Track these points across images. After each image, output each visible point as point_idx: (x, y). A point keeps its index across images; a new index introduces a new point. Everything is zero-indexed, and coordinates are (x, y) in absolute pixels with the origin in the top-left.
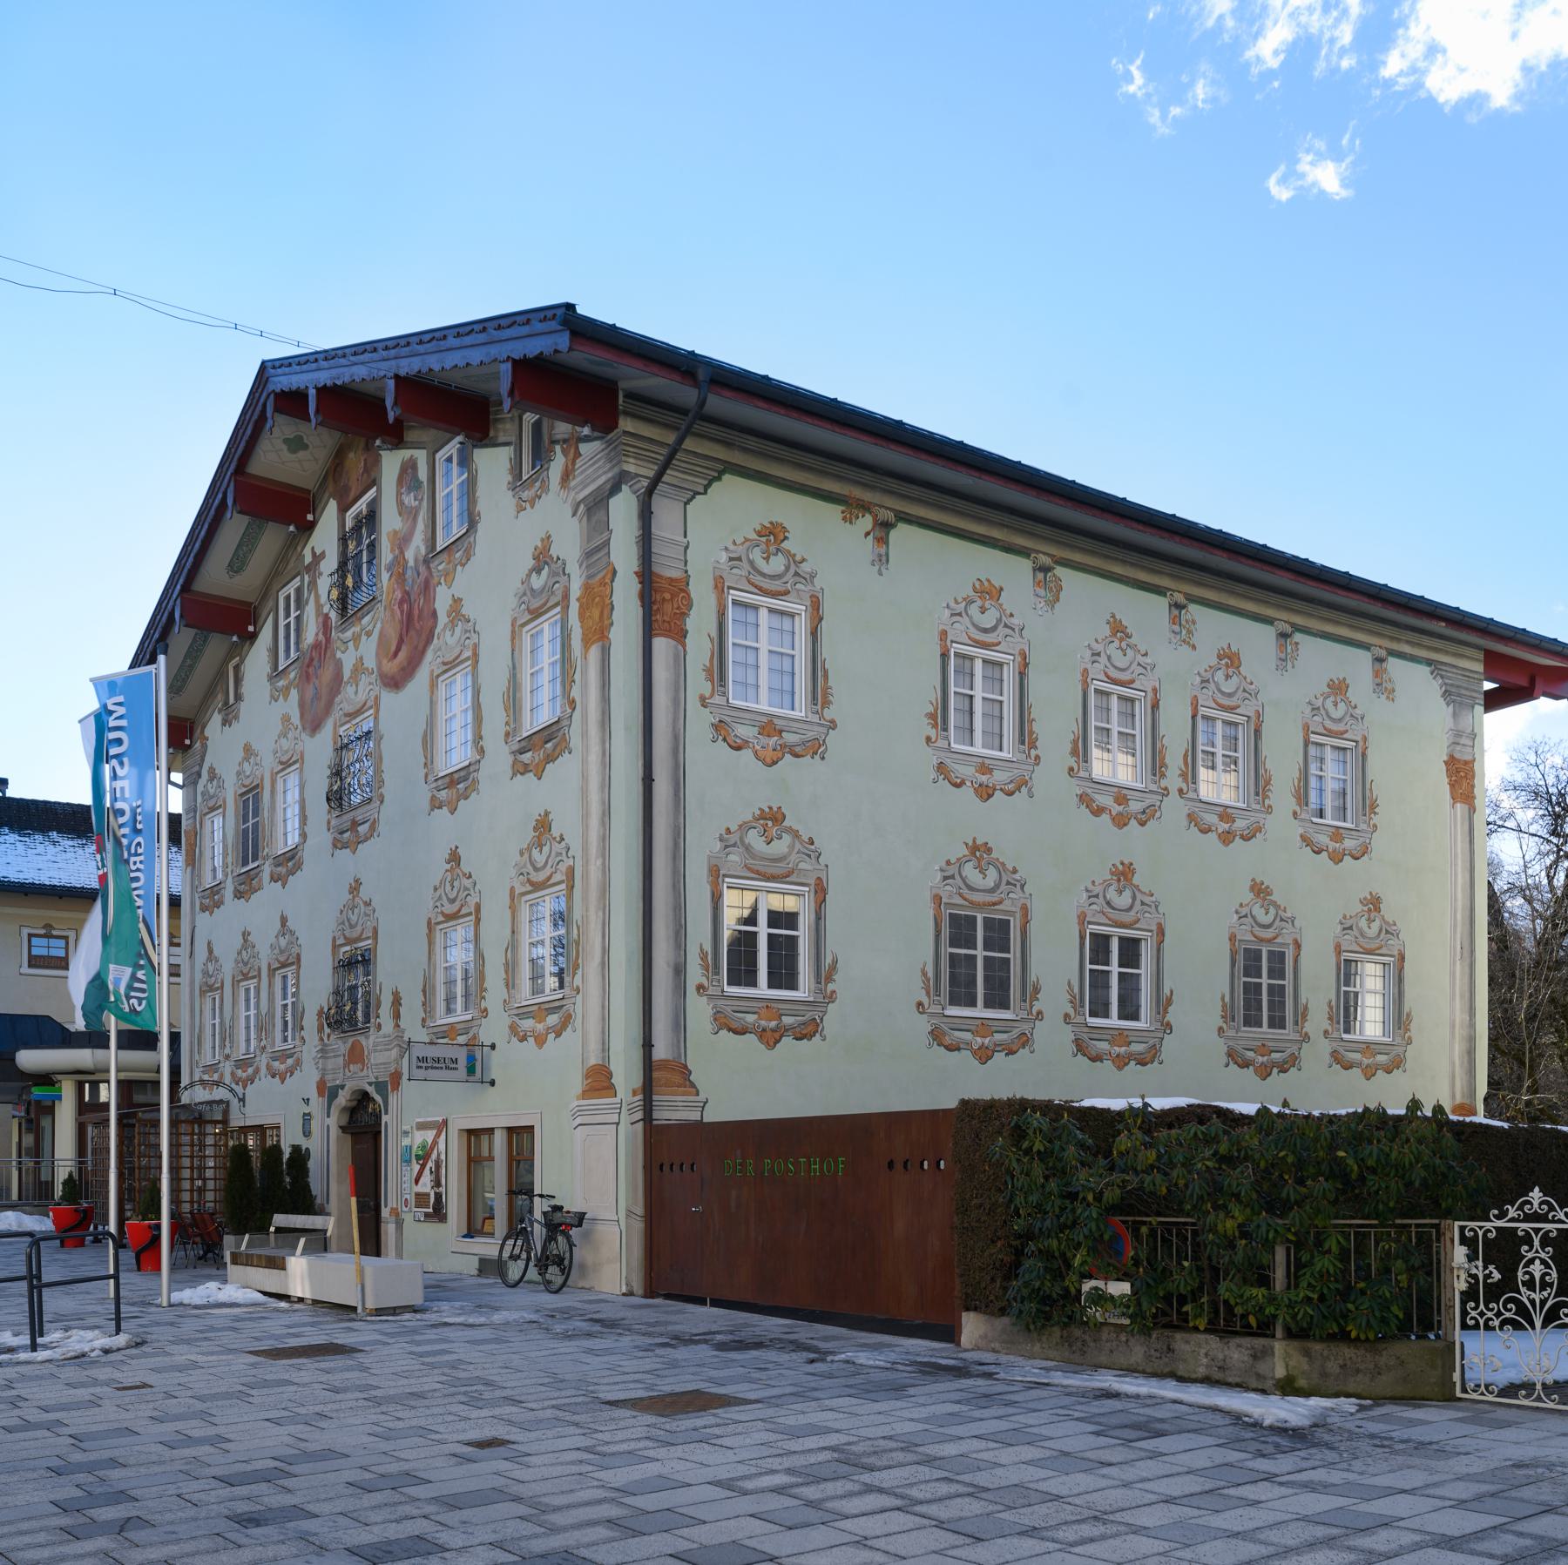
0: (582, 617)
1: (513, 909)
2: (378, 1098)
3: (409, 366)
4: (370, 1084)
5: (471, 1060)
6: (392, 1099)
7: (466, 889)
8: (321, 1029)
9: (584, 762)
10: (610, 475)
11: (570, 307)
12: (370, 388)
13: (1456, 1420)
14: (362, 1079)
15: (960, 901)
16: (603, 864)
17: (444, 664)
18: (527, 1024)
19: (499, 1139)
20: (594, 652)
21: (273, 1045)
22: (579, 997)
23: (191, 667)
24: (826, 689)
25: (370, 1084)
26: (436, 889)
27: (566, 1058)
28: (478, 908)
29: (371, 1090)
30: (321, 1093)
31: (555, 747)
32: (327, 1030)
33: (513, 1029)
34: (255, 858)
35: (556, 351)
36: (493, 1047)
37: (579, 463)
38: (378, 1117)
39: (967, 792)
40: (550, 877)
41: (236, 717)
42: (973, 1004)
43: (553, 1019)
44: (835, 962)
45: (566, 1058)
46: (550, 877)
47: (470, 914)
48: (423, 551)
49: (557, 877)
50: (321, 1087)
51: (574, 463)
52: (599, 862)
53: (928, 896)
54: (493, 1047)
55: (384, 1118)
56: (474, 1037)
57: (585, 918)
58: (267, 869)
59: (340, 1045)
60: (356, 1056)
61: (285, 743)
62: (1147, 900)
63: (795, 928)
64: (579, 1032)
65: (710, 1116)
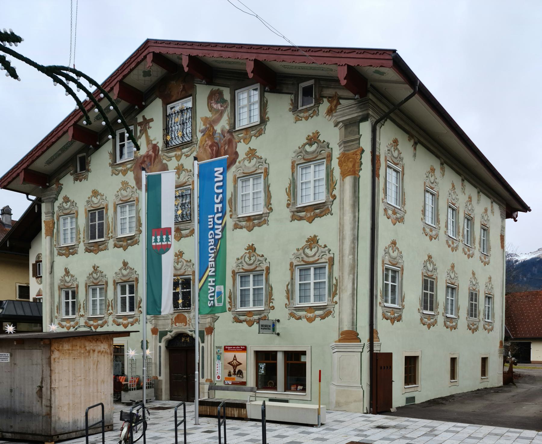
0: (340, 164)
3: (194, 53)
7: (259, 260)
9: (341, 219)
10: (360, 114)
11: (394, 51)
12: (175, 58)
13: (251, 426)
15: (302, 263)
16: (354, 258)
17: (244, 173)
19: (280, 358)
20: (349, 180)
21: (117, 313)
22: (337, 306)
23: (60, 154)
26: (238, 259)
27: (329, 329)
28: (268, 269)
31: (321, 212)
34: (101, 236)
35: (358, 65)
37: (339, 107)
39: (428, 237)
40: (318, 260)
41: (86, 178)
42: (190, 291)
45: (329, 329)
46: (318, 260)
48: (227, 127)
51: (336, 106)
52: (351, 257)
53: (421, 273)
54: (278, 321)
56: (265, 316)
57: (342, 277)
58: (111, 243)
61: (124, 193)
62: (261, 259)
64: (337, 318)
65: (382, 351)
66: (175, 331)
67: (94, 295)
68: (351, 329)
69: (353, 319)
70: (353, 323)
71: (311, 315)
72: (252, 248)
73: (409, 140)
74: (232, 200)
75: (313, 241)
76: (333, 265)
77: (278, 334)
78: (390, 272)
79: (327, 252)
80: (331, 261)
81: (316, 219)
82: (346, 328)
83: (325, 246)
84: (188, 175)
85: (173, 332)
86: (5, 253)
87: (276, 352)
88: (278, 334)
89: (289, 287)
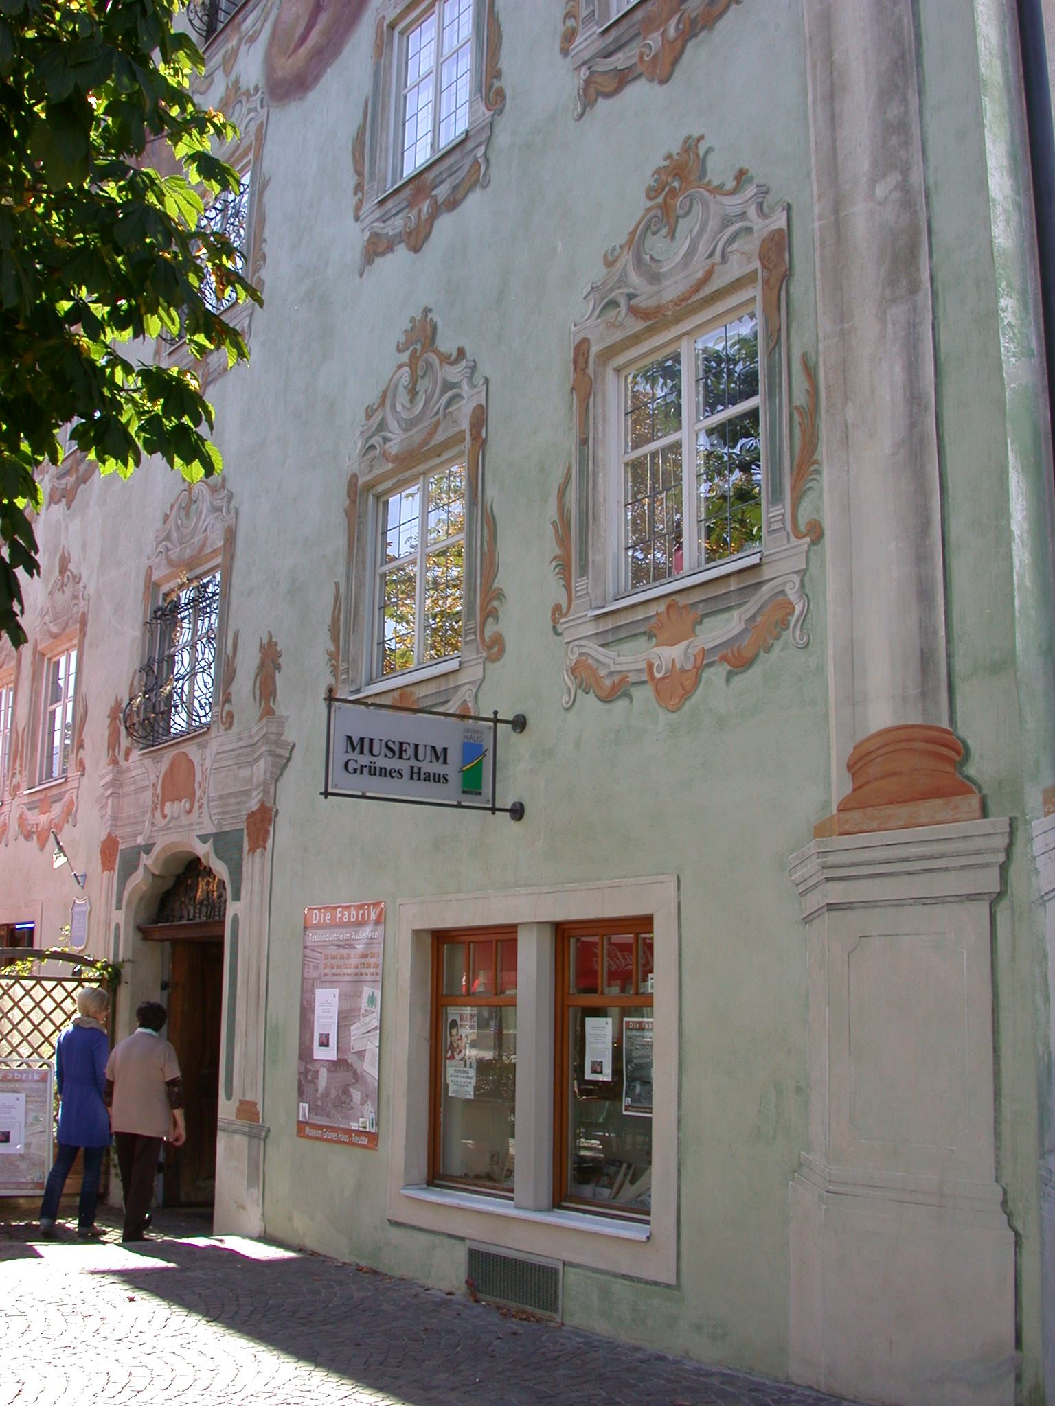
1: (584, 390)
2: (220, 868)
4: (204, 839)
5: (473, 751)
6: (252, 866)
7: (447, 386)
8: (113, 743)
14: (189, 831)
18: (628, 658)
24: (563, 541)
25: (204, 839)
28: (480, 417)
29: (203, 850)
30: (107, 863)
32: (125, 741)
33: (584, 676)
36: (520, 724)
38: (216, 909)
43: (723, 628)
44: (37, 1255)
47: (458, 438)
49: (735, 269)
50: (109, 849)
54: (520, 724)
55: (232, 908)
59: (144, 769)
60: (179, 785)
63: (498, 942)
66: (161, 842)
67: (652, 419)
68: (914, 719)
69: (926, 630)
70: (926, 660)
71: (670, 655)
72: (422, 336)
73: (650, 1045)
74: (363, 134)
75: (680, 178)
76: (787, 276)
77: (517, 812)
78: (428, 550)
79: (752, 211)
80: (777, 251)
81: (690, 44)
82: (881, 715)
83: (742, 176)
84: (250, 111)
85: (156, 850)
86: (571, 407)
87: (512, 929)
88: (517, 812)
89: (572, 495)
